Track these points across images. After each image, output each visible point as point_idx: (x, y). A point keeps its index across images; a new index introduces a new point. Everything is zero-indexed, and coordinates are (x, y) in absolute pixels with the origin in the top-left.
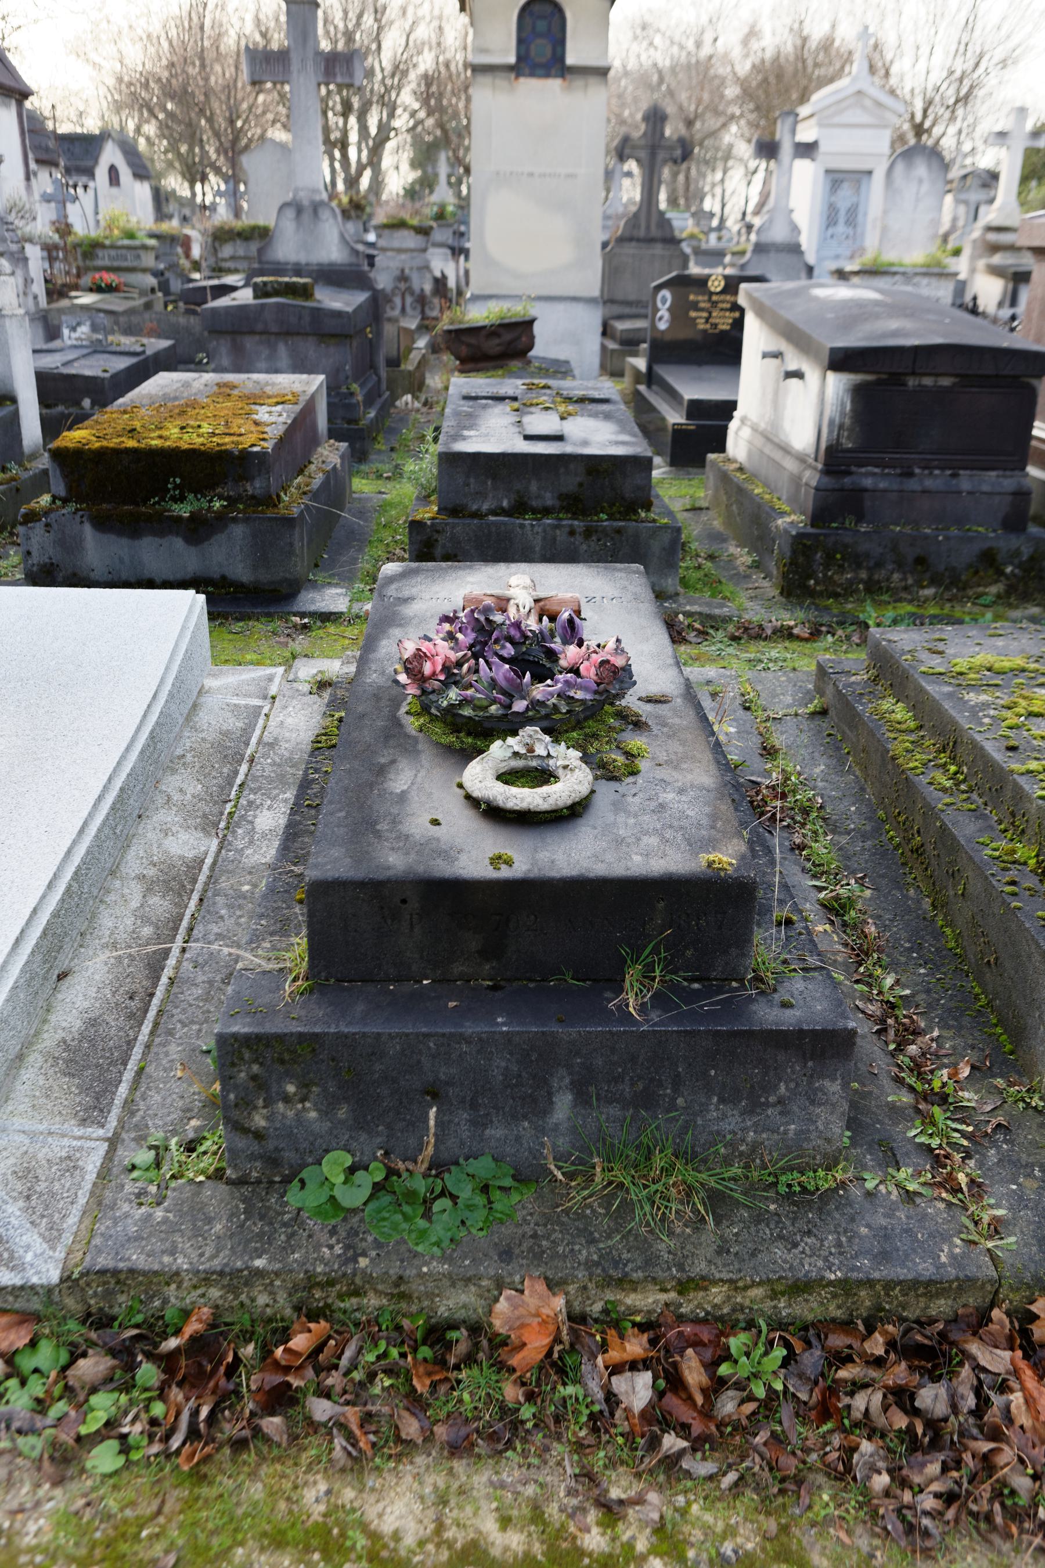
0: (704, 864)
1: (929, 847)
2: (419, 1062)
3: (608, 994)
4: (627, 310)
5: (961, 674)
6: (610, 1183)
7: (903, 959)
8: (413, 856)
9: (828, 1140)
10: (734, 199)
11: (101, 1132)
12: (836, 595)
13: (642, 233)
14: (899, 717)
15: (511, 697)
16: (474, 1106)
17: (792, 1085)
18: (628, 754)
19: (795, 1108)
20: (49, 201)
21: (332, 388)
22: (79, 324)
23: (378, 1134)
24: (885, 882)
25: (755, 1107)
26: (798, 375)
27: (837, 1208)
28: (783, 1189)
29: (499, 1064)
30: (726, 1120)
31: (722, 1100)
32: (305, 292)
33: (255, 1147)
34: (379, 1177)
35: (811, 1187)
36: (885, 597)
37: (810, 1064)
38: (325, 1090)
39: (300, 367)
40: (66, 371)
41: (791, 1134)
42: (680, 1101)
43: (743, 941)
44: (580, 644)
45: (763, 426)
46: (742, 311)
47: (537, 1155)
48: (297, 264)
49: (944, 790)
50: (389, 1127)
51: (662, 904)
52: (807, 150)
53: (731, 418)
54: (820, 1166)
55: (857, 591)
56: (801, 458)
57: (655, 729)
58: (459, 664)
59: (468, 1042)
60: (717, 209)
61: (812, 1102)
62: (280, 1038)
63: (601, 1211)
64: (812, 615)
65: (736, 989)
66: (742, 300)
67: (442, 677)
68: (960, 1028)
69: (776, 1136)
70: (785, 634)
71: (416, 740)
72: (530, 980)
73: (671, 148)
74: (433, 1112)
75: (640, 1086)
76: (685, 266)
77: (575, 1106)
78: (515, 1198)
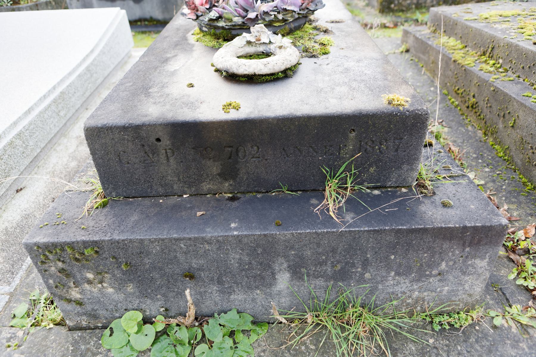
0: (385, 102)
1: (481, 103)
2: (176, 257)
3: (314, 201)
5: (487, 18)
6: (318, 324)
7: (474, 164)
8: (168, 107)
9: (470, 295)
12: (402, 11)
14: (452, 44)
15: (247, 11)
16: (220, 282)
17: (451, 263)
18: (323, 44)
19: (451, 278)
23: (158, 300)
24: (453, 124)
25: (421, 276)
27: (477, 341)
28: (437, 328)
29: (234, 258)
30: (400, 287)
31: (398, 274)
33: (78, 309)
34: (160, 327)
35: (457, 326)
36: (424, 10)
37: (468, 249)
38: (114, 276)
41: (445, 292)
42: (367, 275)
43: (412, 160)
47: (267, 309)
49: (490, 72)
50: (164, 295)
51: (353, 134)
54: (462, 310)
55: (412, 8)
57: (337, 33)
59: (209, 242)
61: (464, 273)
62: (72, 245)
63: (313, 347)
64: (394, 19)
65: (405, 194)
68: (520, 203)
69: (434, 294)
70: (384, 26)
71: (193, 45)
72: (258, 192)
74: (187, 292)
75: (339, 267)
77: (292, 280)
78: (254, 337)
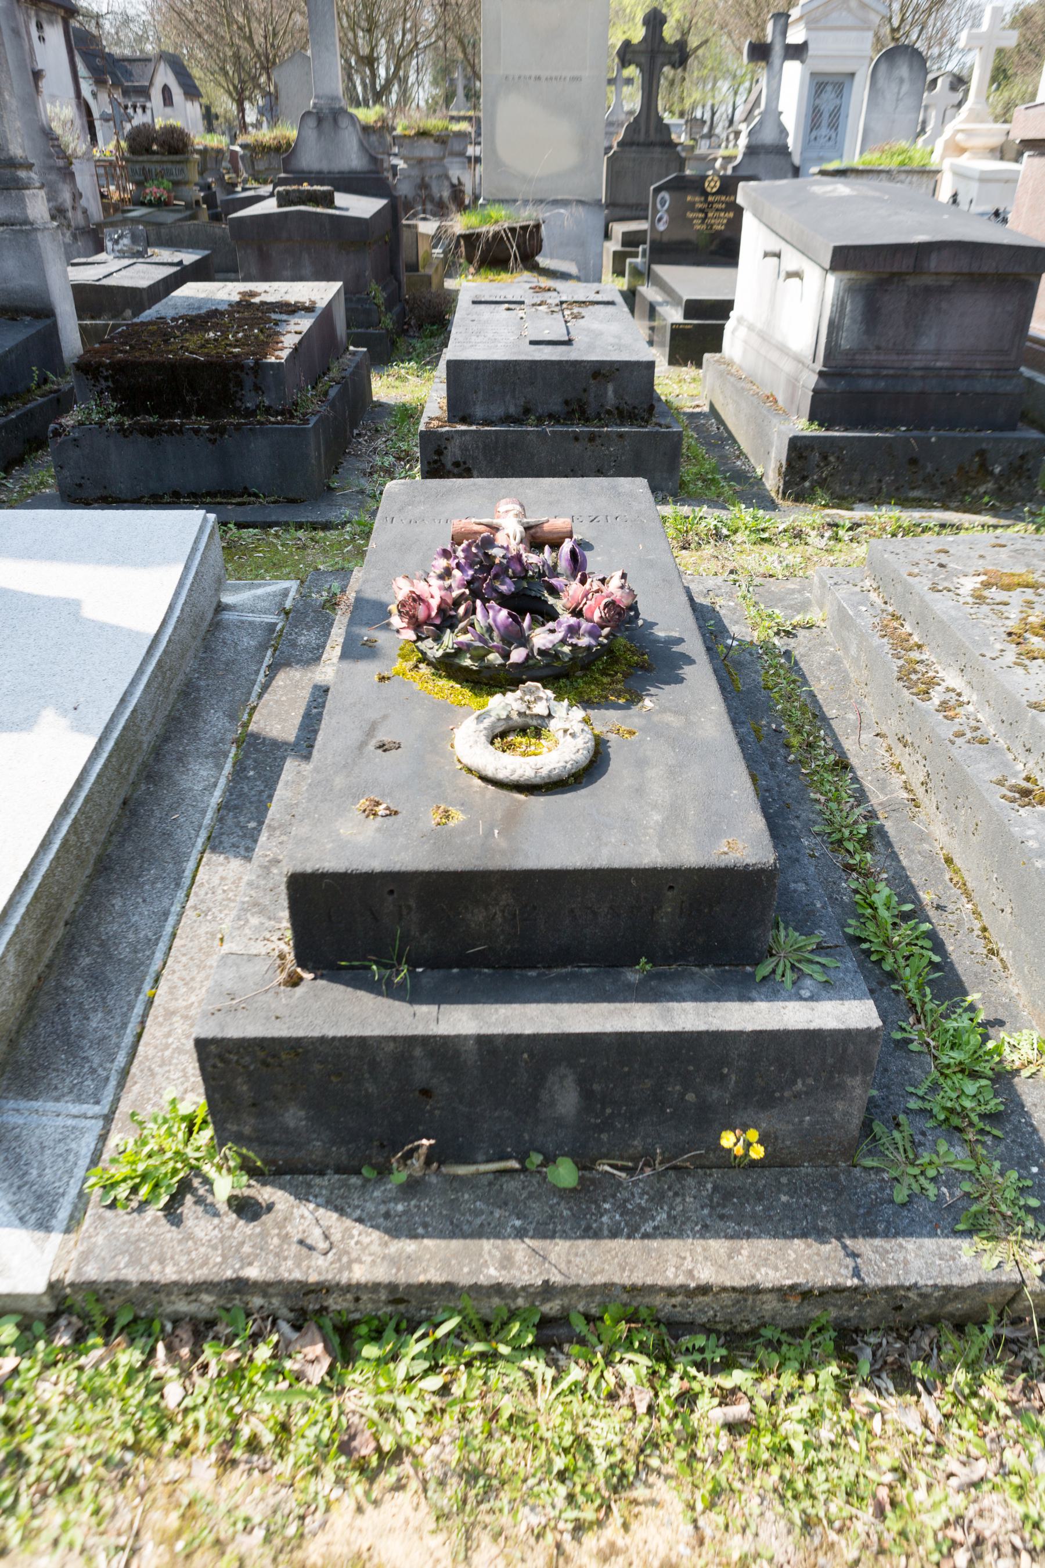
4: (628, 213)
10: (722, 109)
11: (97, 1109)
13: (642, 138)
20: (107, 120)
21: (349, 293)
22: (120, 237)
26: (797, 275)
32: (327, 200)
39: (323, 274)
40: (104, 282)
44: (583, 582)
45: (759, 325)
46: (739, 211)
48: (320, 172)
52: (797, 52)
53: (727, 318)
56: (798, 359)
58: (457, 603)
60: (707, 116)
66: (740, 200)
67: (438, 622)
73: (672, 53)
76: (682, 168)
